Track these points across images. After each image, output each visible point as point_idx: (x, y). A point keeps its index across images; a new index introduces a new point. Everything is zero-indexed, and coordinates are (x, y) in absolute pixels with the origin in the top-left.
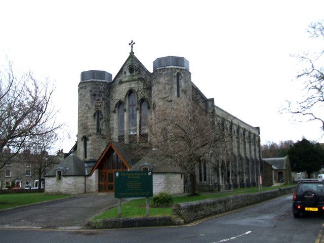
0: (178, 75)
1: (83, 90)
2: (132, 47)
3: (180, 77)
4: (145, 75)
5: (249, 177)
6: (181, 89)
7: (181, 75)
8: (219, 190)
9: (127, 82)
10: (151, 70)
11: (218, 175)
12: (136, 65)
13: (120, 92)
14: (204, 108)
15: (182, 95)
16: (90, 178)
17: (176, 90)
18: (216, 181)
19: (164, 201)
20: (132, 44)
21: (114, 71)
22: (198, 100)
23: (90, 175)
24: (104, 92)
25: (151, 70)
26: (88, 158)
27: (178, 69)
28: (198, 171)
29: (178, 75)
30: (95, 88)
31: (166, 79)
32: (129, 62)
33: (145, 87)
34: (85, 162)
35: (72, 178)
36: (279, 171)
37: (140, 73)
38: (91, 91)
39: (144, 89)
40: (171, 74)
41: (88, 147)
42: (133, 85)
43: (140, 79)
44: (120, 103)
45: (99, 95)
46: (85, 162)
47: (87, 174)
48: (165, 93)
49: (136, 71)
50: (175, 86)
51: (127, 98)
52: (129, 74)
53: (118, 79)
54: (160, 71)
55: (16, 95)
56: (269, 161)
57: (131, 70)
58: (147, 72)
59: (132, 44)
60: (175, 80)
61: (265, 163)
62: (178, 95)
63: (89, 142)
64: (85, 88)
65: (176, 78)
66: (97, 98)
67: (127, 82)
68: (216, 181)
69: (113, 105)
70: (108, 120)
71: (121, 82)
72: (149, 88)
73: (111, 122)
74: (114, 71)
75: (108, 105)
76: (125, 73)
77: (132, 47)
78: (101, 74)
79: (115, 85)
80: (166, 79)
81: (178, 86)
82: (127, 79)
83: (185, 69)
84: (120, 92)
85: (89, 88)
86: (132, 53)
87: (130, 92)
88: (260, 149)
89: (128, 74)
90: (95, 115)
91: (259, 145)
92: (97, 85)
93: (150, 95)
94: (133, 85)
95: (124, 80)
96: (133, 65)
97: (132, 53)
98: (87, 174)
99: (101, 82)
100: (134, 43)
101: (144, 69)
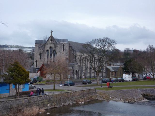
0: (64, 45)
1: (36, 46)
2: (52, 33)
5: (95, 74)
6: (64, 49)
9: (49, 44)
13: (48, 47)
14: (73, 53)
15: (64, 51)
16: (37, 73)
19: (35, 81)
20: (52, 32)
22: (72, 51)
23: (37, 73)
26: (37, 67)
27: (63, 43)
29: (64, 45)
30: (40, 46)
32: (51, 38)
34: (36, 68)
35: (32, 73)
39: (54, 47)
40: (61, 44)
41: (37, 64)
42: (52, 45)
43: (54, 44)
44: (48, 51)
45: (41, 48)
46: (36, 68)
47: (36, 72)
48: (59, 50)
50: (62, 48)
52: (51, 42)
57: (51, 40)
59: (52, 32)
60: (63, 47)
62: (63, 51)
63: (37, 62)
64: (37, 45)
65: (63, 46)
66: (40, 49)
67: (49, 44)
68: (72, 77)
69: (45, 51)
70: (43, 56)
72: (56, 47)
73: (45, 56)
75: (44, 51)
77: (52, 33)
81: (63, 48)
82: (50, 43)
84: (48, 47)
85: (38, 46)
86: (51, 35)
87: (51, 47)
90: (39, 54)
94: (52, 45)
95: (49, 43)
96: (52, 39)
97: (51, 35)
98: (36, 72)
100: (52, 32)
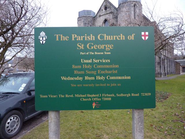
3: (136, 7)
4: (114, 10)
7: (136, 5)
8: (161, 76)
10: (117, 6)
11: (160, 67)
12: (108, 5)
17: (133, 15)
18: (159, 71)
21: (95, 10)
24: (90, 22)
25: (117, 6)
28: (15, 111)
31: (127, 8)
33: (114, 17)
36: (183, 66)
37: (111, 9)
38: (83, 22)
39: (113, 18)
43: (111, 13)
49: (108, 8)
50: (133, 13)
51: (104, 24)
53: (99, 14)
54: (123, 4)
55: (164, 116)
56: (178, 61)
58: (115, 8)
60: (133, 9)
61: (176, 62)
62: (135, 18)
71: (100, 16)
72: (116, 18)
74: (95, 10)
76: (102, 10)
78: (89, 12)
79: (97, 18)
80: (127, 8)
82: (103, 14)
83: (139, 2)
84: (100, 22)
87: (106, 21)
88: (173, 55)
89: (104, 10)
91: (173, 53)
92: (87, 18)
93: (117, 21)
94: (107, 17)
99: (89, 16)
101: (113, 6)
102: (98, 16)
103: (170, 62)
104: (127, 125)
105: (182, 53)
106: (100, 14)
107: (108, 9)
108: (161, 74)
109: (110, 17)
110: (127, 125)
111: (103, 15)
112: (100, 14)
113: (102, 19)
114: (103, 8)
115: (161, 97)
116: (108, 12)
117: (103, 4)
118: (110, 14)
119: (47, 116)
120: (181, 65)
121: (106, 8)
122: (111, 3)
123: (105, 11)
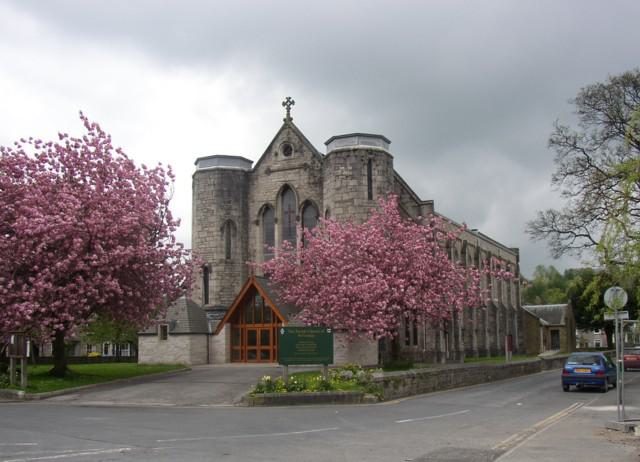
11: (438, 335)
12: (295, 140)
21: (255, 156)
33: (312, 181)
43: (305, 167)
49: (296, 151)
51: (280, 197)
53: (264, 166)
58: (315, 154)
62: (370, 196)
71: (269, 172)
76: (276, 154)
87: (286, 189)
89: (282, 157)
93: (321, 195)
102: (262, 170)
103: (494, 316)
104: (366, 237)
105: (600, 246)
106: (269, 164)
107: (293, 155)
108: (438, 354)
109: (299, 180)
110: (366, 237)
111: (278, 171)
112: (269, 164)
113: (276, 181)
114: (278, 148)
115: (56, 160)
116: (296, 164)
117: (280, 137)
118: (302, 171)
119: (540, 283)
120: (541, 325)
121: (287, 150)
122: (302, 135)
123: (284, 157)
